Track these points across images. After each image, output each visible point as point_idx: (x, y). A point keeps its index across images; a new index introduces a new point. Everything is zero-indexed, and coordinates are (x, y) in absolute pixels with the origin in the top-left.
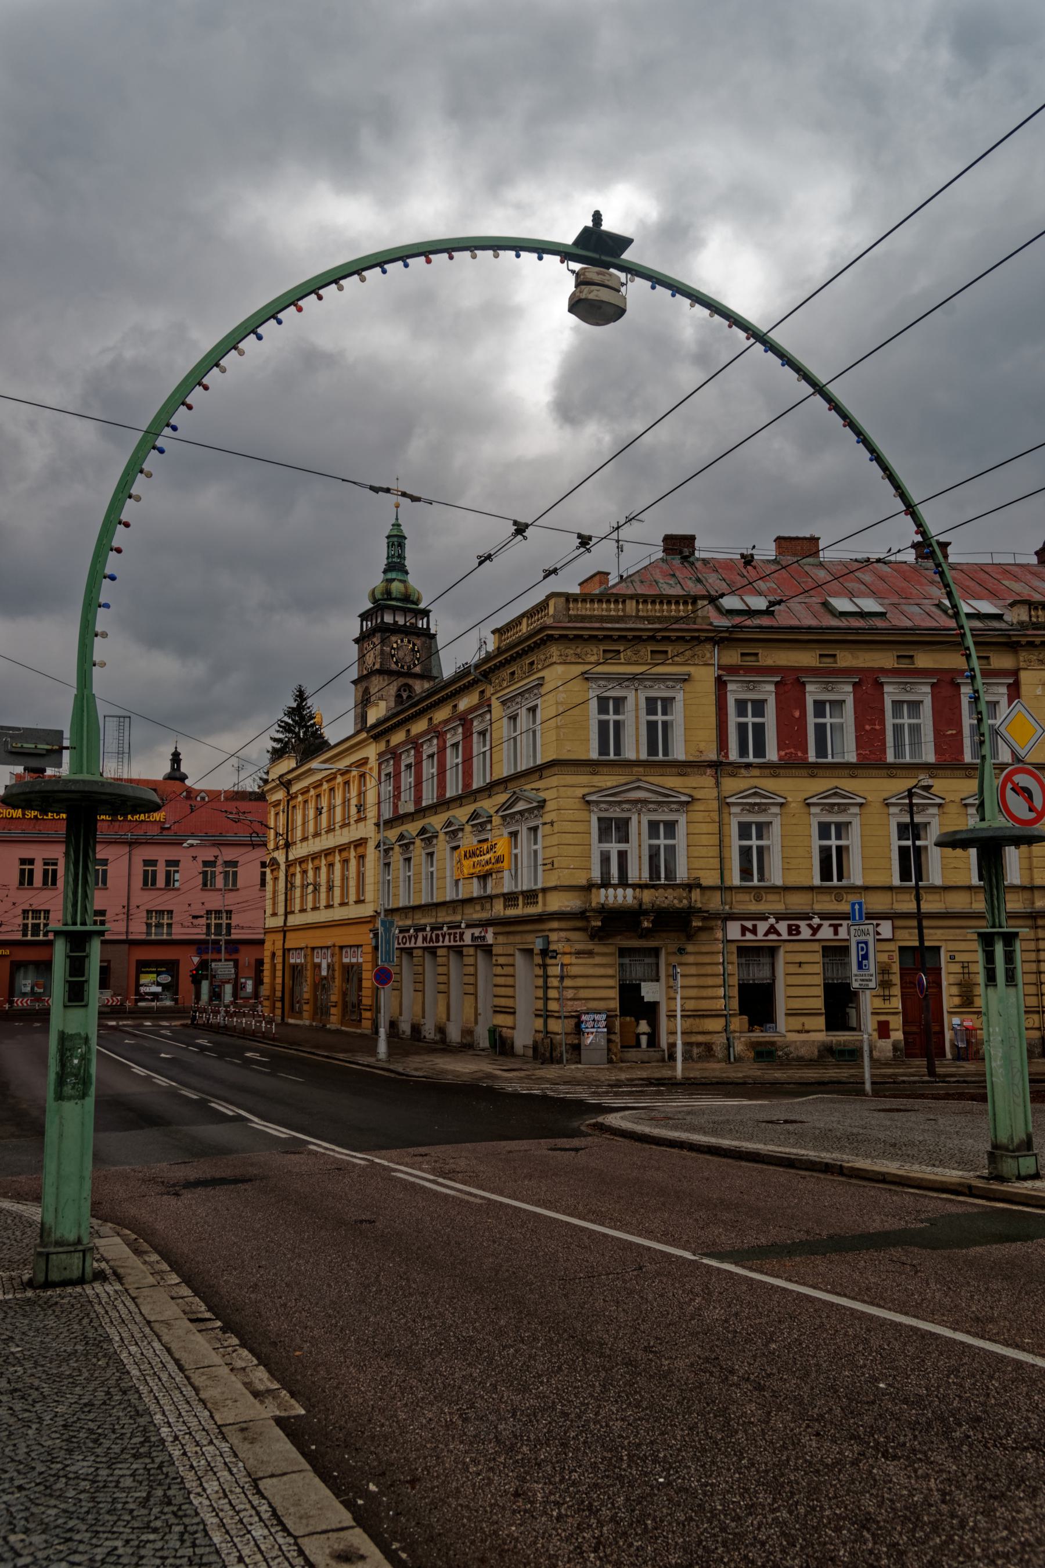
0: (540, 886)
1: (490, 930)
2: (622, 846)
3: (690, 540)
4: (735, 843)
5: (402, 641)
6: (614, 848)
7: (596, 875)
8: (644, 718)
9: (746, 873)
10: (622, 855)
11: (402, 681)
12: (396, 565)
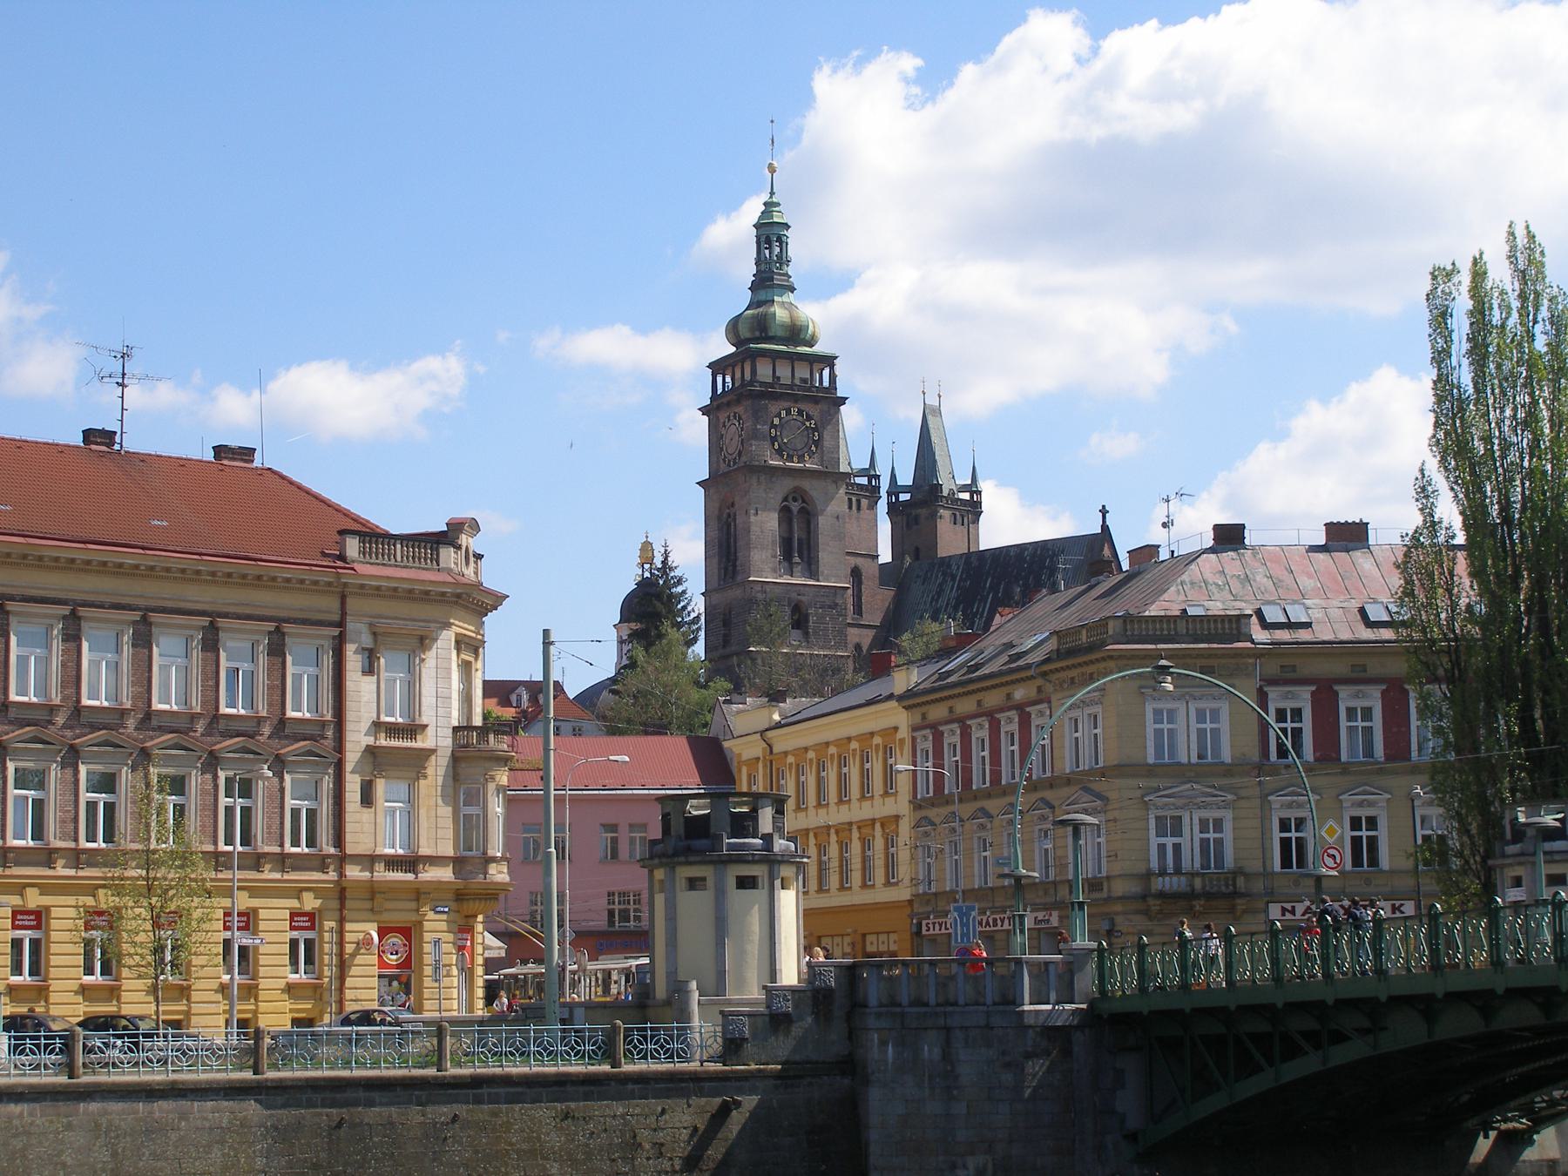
0: (1104, 874)
1: (1055, 914)
2: (1176, 840)
3: (1240, 528)
4: (1277, 835)
5: (788, 412)
6: (1169, 841)
7: (1154, 864)
8: (1194, 726)
9: (1286, 862)
10: (1177, 847)
11: (788, 484)
12: (770, 276)
